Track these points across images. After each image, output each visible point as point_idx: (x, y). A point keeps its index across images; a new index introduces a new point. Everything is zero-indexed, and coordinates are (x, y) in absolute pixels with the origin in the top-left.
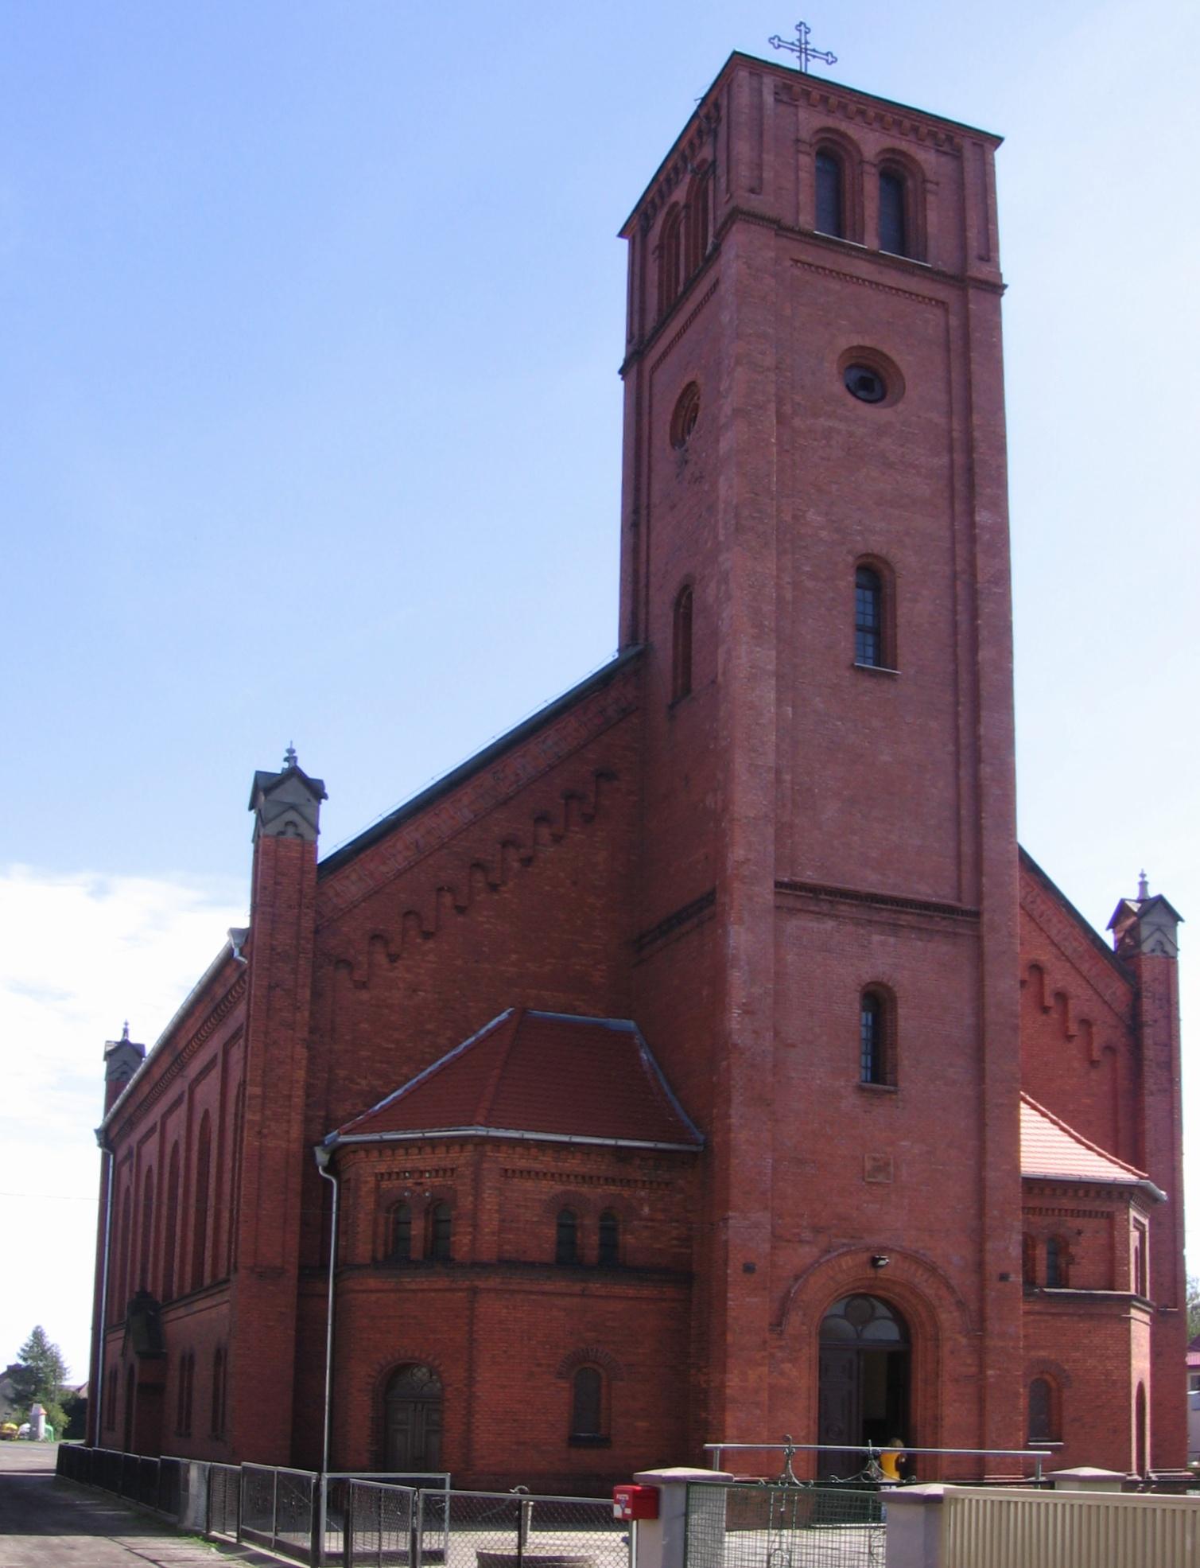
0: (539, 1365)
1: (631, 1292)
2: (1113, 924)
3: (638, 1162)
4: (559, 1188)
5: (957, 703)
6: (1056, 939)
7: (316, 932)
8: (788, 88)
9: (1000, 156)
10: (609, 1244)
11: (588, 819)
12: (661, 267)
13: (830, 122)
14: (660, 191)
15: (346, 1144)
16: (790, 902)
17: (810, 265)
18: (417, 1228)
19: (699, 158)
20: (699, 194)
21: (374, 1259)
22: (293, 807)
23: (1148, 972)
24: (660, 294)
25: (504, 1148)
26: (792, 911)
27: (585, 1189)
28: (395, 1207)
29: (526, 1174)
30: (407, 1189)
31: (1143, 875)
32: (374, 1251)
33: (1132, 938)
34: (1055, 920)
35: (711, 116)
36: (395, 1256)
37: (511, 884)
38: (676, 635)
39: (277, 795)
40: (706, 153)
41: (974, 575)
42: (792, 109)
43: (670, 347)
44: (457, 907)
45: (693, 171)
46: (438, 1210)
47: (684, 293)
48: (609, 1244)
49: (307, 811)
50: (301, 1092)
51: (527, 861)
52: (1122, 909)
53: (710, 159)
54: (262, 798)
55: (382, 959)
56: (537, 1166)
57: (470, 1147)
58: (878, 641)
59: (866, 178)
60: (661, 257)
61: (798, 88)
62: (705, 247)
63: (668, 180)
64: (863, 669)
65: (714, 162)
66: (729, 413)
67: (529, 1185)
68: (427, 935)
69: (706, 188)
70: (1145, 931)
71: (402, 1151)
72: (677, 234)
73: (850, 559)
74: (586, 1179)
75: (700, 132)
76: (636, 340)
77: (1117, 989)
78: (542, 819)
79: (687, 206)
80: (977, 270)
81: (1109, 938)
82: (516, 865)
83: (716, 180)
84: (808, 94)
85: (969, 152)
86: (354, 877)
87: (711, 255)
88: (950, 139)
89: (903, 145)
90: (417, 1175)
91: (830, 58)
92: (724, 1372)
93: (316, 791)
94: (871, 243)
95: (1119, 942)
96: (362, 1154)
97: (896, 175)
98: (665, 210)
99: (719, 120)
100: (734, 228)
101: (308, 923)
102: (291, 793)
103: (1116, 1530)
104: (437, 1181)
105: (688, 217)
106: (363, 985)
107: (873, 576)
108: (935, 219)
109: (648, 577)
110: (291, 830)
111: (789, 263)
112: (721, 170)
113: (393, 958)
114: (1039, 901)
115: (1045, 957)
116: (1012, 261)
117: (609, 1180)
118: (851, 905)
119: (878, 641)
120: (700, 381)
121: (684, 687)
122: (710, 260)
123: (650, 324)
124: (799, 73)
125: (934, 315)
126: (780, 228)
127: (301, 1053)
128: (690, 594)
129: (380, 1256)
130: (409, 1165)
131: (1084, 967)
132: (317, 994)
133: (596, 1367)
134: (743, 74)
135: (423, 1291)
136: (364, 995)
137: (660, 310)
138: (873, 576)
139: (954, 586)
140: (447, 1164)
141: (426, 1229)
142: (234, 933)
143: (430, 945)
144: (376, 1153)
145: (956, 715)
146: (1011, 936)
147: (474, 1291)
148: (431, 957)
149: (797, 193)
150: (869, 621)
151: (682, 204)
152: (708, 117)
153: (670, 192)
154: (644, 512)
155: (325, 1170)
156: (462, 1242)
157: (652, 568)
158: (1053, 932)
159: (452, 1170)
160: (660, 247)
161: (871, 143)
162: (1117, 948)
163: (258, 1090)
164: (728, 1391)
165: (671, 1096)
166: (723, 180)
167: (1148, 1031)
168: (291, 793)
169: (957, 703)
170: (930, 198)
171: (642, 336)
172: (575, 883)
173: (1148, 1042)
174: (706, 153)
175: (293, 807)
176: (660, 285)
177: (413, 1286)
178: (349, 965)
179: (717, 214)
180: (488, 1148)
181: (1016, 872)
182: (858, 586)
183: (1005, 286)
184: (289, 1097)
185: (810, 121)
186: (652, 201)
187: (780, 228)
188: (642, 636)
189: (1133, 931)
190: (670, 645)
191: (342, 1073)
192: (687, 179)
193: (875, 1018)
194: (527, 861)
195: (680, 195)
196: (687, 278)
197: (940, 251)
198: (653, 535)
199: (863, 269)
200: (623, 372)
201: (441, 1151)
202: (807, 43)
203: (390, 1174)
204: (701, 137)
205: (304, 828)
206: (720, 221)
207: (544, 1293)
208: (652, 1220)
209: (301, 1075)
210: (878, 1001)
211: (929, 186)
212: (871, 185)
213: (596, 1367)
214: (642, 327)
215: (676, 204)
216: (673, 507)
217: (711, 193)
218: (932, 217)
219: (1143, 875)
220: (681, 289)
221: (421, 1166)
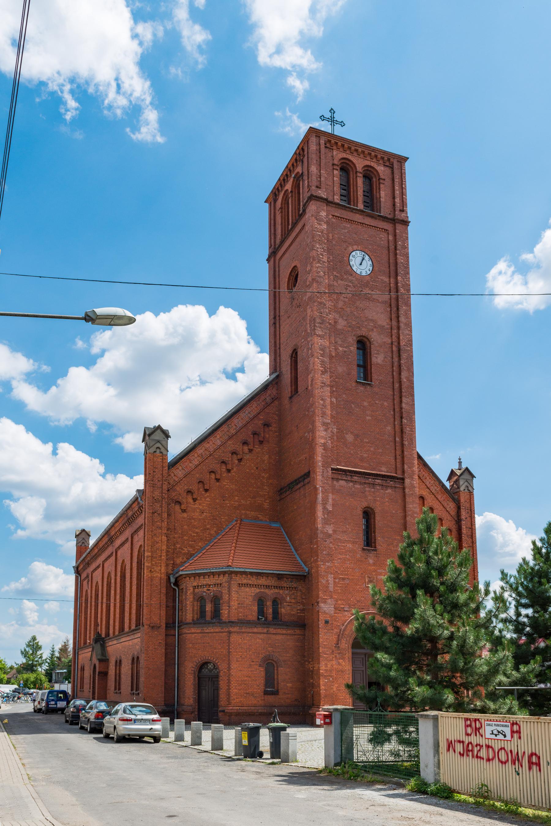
0: (253, 662)
1: (284, 632)
2: (449, 479)
3: (285, 579)
4: (258, 590)
5: (394, 395)
6: (429, 486)
7: (168, 491)
8: (330, 141)
9: (408, 165)
10: (276, 613)
11: (261, 442)
12: (282, 217)
13: (345, 156)
14: (281, 184)
15: (181, 575)
16: (335, 476)
17: (338, 217)
18: (209, 608)
19: (296, 171)
20: (297, 186)
21: (193, 620)
22: (158, 442)
23: (463, 499)
24: (282, 228)
25: (238, 575)
26: (338, 480)
27: (267, 591)
28: (201, 600)
29: (246, 585)
30: (204, 592)
31: (460, 459)
32: (193, 617)
33: (457, 485)
34: (428, 478)
35: (301, 154)
36: (201, 619)
37: (235, 469)
38: (291, 369)
39: (153, 437)
40: (299, 169)
41: (399, 343)
42: (331, 150)
43: (286, 251)
44: (216, 479)
45: (294, 178)
46: (216, 600)
47: (292, 228)
48: (276, 613)
49: (164, 443)
50: (165, 554)
51: (240, 460)
52: (452, 473)
53: (301, 172)
54: (147, 438)
55: (191, 501)
56: (250, 582)
57: (227, 575)
58: (365, 367)
59: (358, 179)
60: (282, 212)
61: (333, 142)
62: (299, 211)
63: (284, 180)
64: (360, 382)
65: (302, 173)
66: (311, 280)
67: (247, 589)
68: (206, 491)
69: (299, 184)
70: (461, 482)
71: (202, 577)
72: (288, 202)
73: (355, 338)
74: (268, 587)
75: (296, 160)
76: (273, 247)
77: (451, 506)
78: (245, 443)
79: (291, 192)
80: (400, 216)
81: (448, 485)
82: (237, 461)
83: (303, 181)
84: (336, 143)
85: (396, 165)
86: (180, 468)
87: (302, 214)
88: (389, 160)
89: (372, 164)
90: (208, 586)
91: (342, 124)
92: (319, 663)
93: (166, 435)
94: (361, 206)
95: (452, 486)
96: (188, 578)
97: (369, 175)
98: (283, 192)
99: (304, 156)
100: (311, 203)
101: (165, 487)
102: (158, 436)
103: (509, 781)
104: (215, 589)
105: (292, 196)
106: (184, 511)
107: (363, 344)
108: (384, 194)
109: (280, 345)
110: (158, 451)
111: (331, 216)
112: (305, 177)
113: (195, 500)
114: (422, 470)
115: (425, 493)
116: (412, 212)
117: (276, 587)
118: (358, 477)
119: (365, 367)
120: (298, 266)
121: (295, 391)
122: (301, 216)
123: (278, 241)
124: (331, 134)
125: (383, 235)
126: (327, 202)
127: (164, 538)
128: (297, 352)
129: (195, 619)
130: (205, 583)
131: (439, 497)
132: (169, 515)
133: (272, 662)
134: (313, 140)
135: (211, 633)
136: (185, 515)
137: (282, 235)
138: (363, 344)
139: (392, 347)
140: (219, 582)
141: (211, 608)
142: (138, 491)
143: (208, 494)
144: (193, 578)
145: (394, 399)
146: (414, 484)
147: (230, 632)
148: (208, 499)
149: (330, 185)
150: (361, 363)
151: (290, 190)
152: (299, 154)
153: (285, 185)
154: (277, 318)
155: (174, 584)
156: (224, 612)
157: (281, 342)
158: (427, 483)
159: (221, 584)
160: (281, 208)
161: (360, 163)
162: (451, 489)
163: (150, 554)
164: (321, 671)
165: (295, 553)
166: (306, 182)
167: (463, 522)
168: (158, 436)
169: (394, 395)
170: (382, 186)
171: (275, 245)
172: (257, 468)
173: (464, 527)
174: (299, 169)
175: (158, 442)
176: (282, 224)
177: (207, 631)
178: (179, 503)
179: (304, 195)
180: (233, 575)
181: (416, 462)
182: (358, 348)
183: (410, 222)
184: (161, 556)
185: (339, 155)
186: (278, 189)
187: (327, 202)
188: (278, 369)
189: (457, 482)
190: (289, 373)
191: (178, 546)
192: (292, 180)
193: (367, 521)
194: (240, 460)
195: (288, 186)
196: (292, 222)
197: (385, 210)
198: (282, 327)
199: (358, 218)
200: (268, 260)
201: (216, 577)
202: (334, 118)
203: (198, 586)
204: (297, 162)
205: (163, 450)
206: (305, 201)
207: (254, 633)
208: (291, 603)
209: (164, 547)
210: (368, 514)
211: (381, 181)
212: (360, 181)
213: (272, 662)
214: (275, 242)
215: (287, 190)
216: (289, 317)
217: (301, 186)
218: (383, 194)
219: (460, 459)
220: (290, 227)
221: (209, 583)
